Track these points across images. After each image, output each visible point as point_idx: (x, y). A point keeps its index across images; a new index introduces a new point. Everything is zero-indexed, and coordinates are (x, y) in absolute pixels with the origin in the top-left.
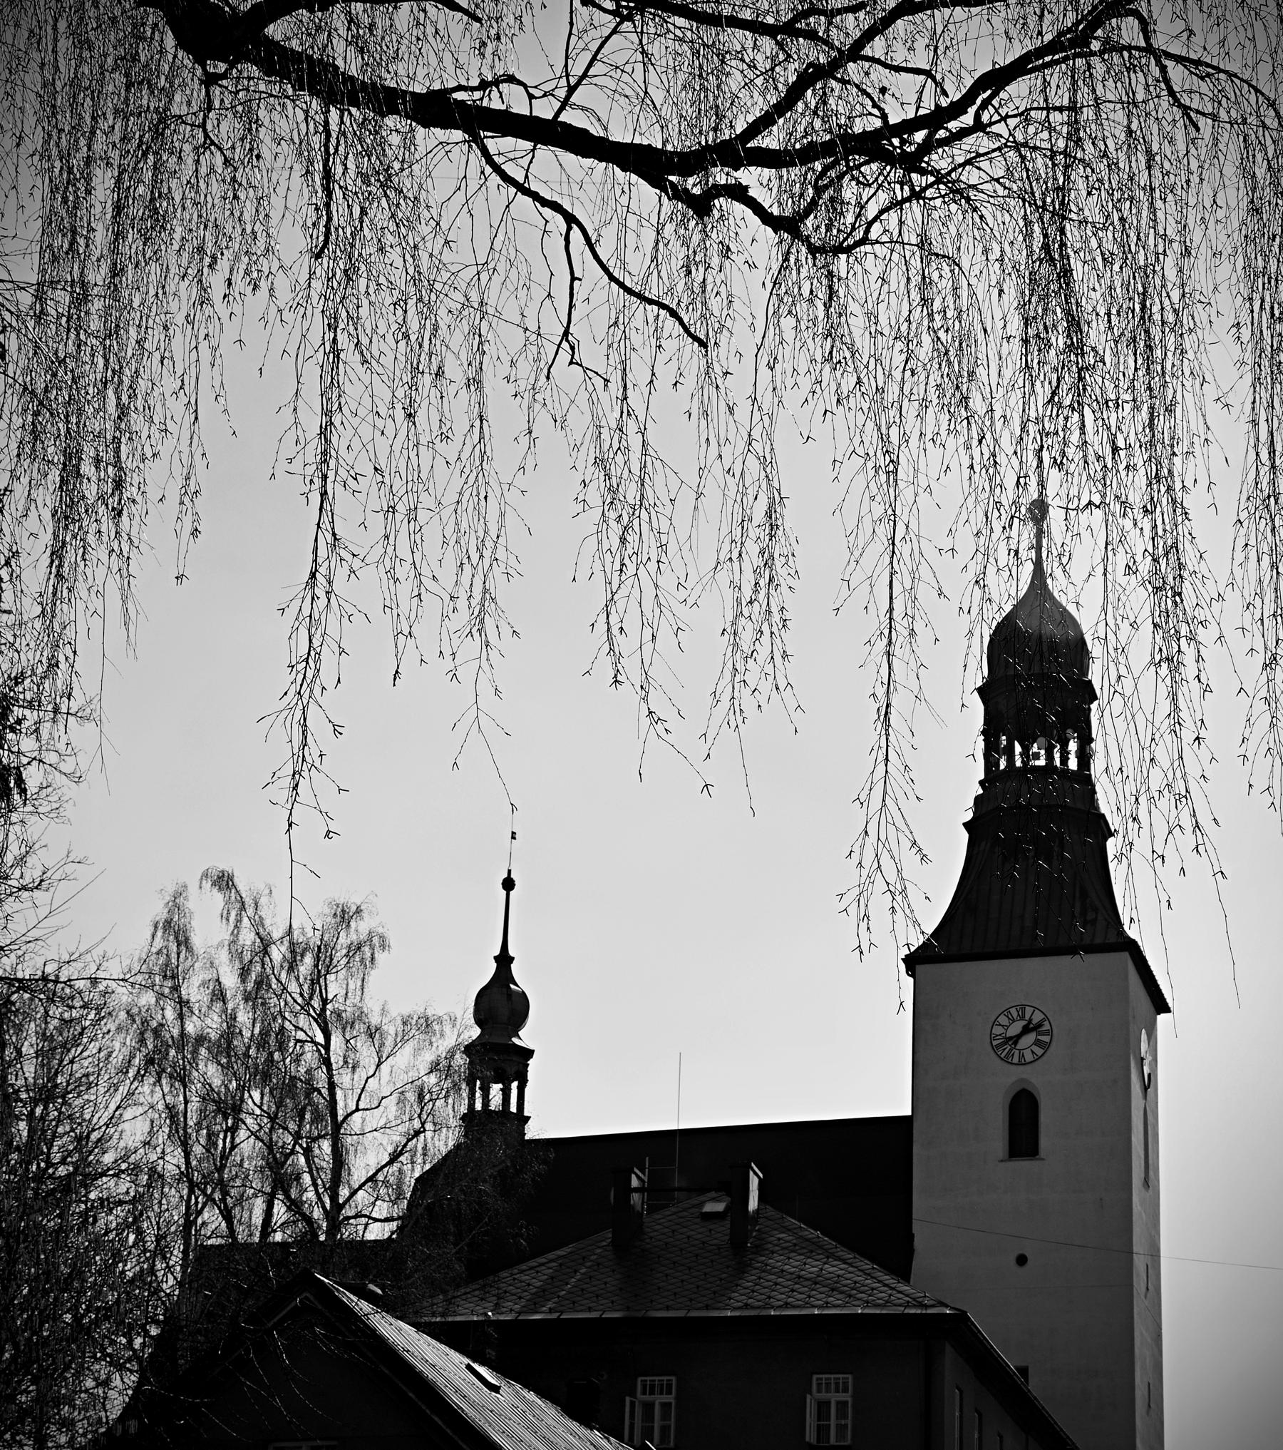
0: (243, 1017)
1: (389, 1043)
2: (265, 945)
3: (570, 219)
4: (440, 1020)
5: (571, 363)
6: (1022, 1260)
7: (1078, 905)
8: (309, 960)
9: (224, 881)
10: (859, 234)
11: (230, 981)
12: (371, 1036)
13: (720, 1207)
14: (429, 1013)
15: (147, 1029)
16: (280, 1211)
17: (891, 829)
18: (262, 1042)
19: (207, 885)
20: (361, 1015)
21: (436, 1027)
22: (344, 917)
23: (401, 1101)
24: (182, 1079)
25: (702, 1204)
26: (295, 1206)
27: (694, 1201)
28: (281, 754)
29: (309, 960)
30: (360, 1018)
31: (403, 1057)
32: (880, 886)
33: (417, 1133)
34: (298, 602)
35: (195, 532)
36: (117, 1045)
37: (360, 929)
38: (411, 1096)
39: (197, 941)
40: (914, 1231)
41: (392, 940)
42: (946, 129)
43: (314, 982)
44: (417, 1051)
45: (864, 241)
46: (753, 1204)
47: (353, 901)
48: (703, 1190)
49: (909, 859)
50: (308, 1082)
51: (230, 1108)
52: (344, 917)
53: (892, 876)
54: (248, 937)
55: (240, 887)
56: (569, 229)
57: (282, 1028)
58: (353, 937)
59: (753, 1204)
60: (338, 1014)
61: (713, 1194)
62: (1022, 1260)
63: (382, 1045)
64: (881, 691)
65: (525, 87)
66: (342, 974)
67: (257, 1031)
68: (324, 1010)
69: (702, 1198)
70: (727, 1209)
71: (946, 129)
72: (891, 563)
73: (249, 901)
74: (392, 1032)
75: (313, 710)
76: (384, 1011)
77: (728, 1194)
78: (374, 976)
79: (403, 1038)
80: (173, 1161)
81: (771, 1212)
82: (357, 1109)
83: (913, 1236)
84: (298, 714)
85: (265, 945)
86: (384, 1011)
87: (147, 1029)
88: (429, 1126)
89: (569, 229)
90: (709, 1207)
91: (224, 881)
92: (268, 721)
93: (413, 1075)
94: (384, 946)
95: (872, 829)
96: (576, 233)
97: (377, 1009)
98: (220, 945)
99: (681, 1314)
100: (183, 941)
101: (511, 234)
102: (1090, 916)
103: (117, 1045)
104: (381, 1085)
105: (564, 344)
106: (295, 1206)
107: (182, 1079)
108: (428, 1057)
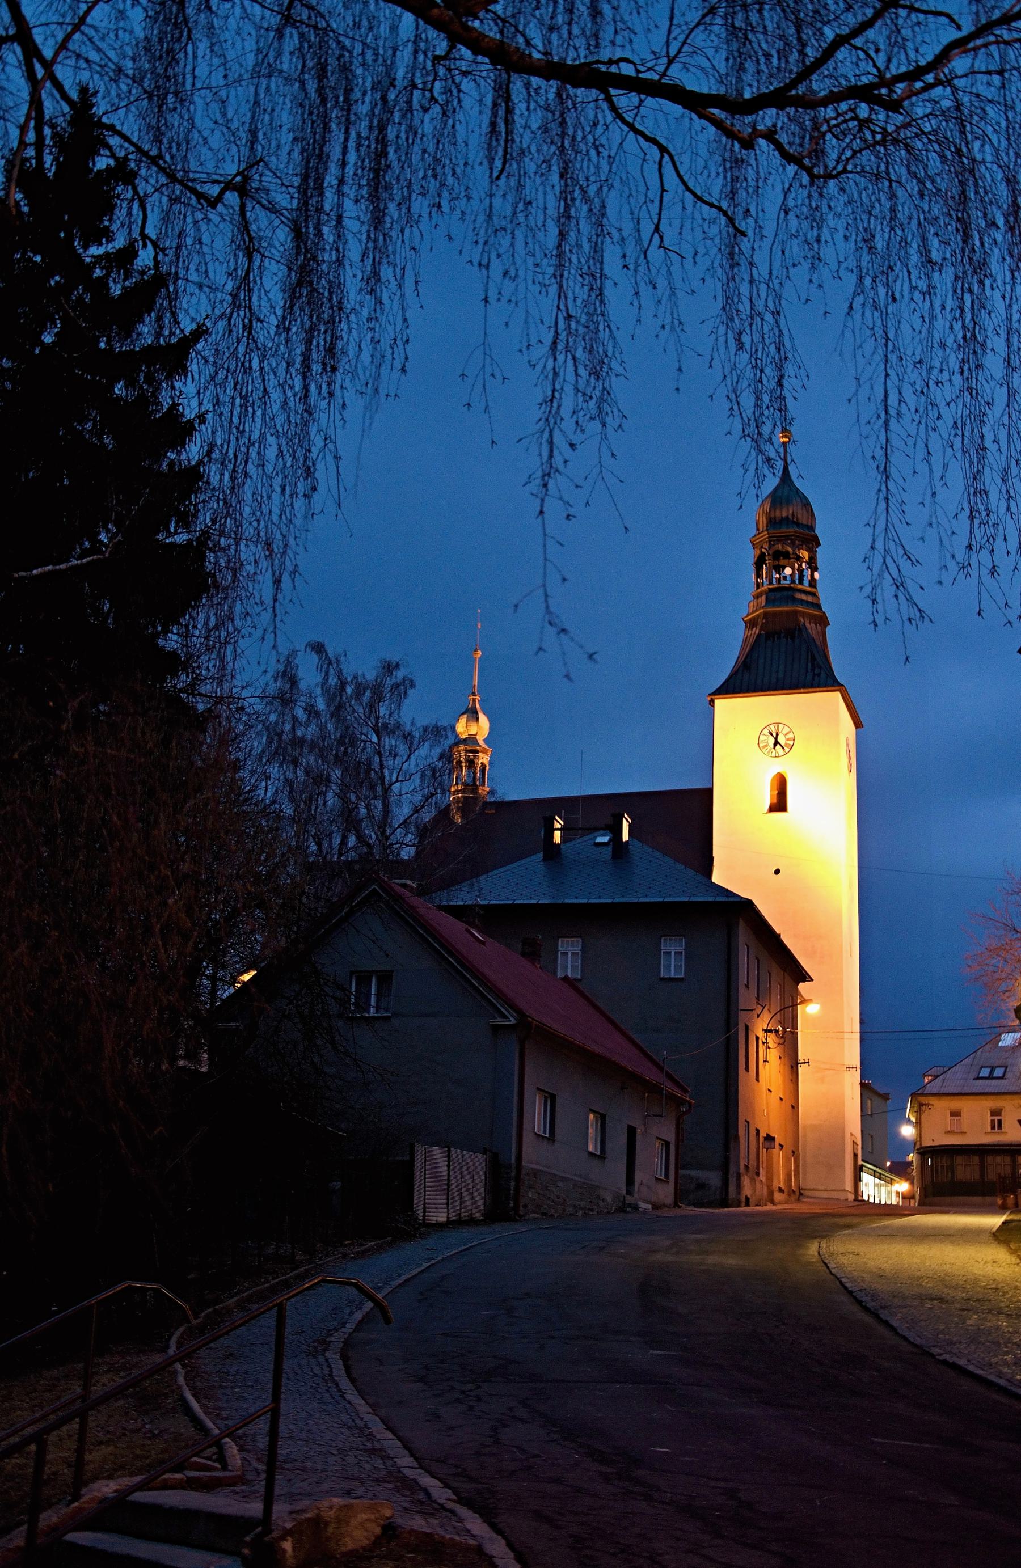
0: (330, 727)
1: (416, 741)
2: (343, 684)
3: (663, 149)
4: (445, 728)
5: (660, 247)
6: (777, 872)
7: (810, 665)
8: (368, 693)
9: (319, 648)
10: (840, 168)
11: (321, 705)
12: (406, 738)
13: (606, 839)
14: (439, 724)
15: (274, 733)
16: (352, 841)
17: (892, 543)
18: (341, 741)
19: (308, 650)
20: (398, 726)
21: (443, 733)
22: (389, 668)
23: (423, 777)
24: (295, 762)
25: (596, 838)
26: (361, 838)
27: (590, 836)
28: (534, 463)
29: (368, 693)
30: (398, 728)
31: (423, 750)
32: (888, 580)
33: (432, 795)
34: (543, 360)
35: (403, 370)
36: (256, 744)
37: (400, 674)
38: (428, 773)
39: (303, 685)
40: (714, 854)
41: (418, 682)
42: (923, 81)
43: (371, 706)
44: (431, 747)
45: (845, 171)
46: (625, 837)
47: (395, 658)
48: (596, 829)
49: (905, 565)
50: (369, 765)
51: (321, 780)
52: (389, 668)
53: (895, 573)
54: (333, 681)
55: (329, 652)
56: (662, 157)
57: (353, 733)
58: (394, 681)
59: (625, 837)
60: (385, 725)
61: (602, 832)
62: (777, 872)
63: (411, 744)
64: (879, 453)
65: (635, 64)
66: (387, 703)
67: (338, 735)
68: (377, 723)
69: (596, 834)
70: (610, 840)
71: (923, 81)
72: (886, 369)
73: (334, 660)
74: (417, 735)
75: (557, 433)
76: (413, 724)
77: (611, 832)
78: (406, 703)
79: (423, 740)
80: (288, 810)
81: (636, 843)
82: (397, 781)
83: (712, 859)
84: (546, 435)
85: (343, 684)
86: (413, 724)
87: (274, 733)
88: (439, 791)
89: (662, 157)
90: (600, 840)
91: (319, 648)
92: (527, 440)
93: (429, 761)
94: (412, 685)
95: (879, 545)
96: (666, 158)
97: (409, 723)
98: (317, 685)
99: (584, 901)
100: (294, 682)
101: (623, 160)
102: (817, 671)
103: (256, 744)
104: (411, 766)
105: (656, 235)
106: (361, 838)
107: (295, 762)
108: (438, 750)
